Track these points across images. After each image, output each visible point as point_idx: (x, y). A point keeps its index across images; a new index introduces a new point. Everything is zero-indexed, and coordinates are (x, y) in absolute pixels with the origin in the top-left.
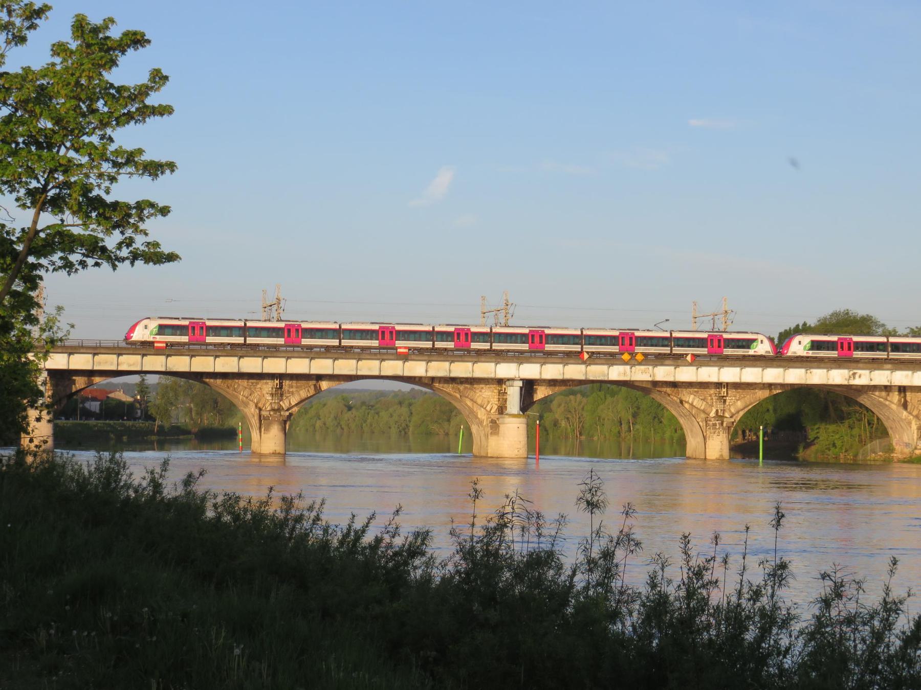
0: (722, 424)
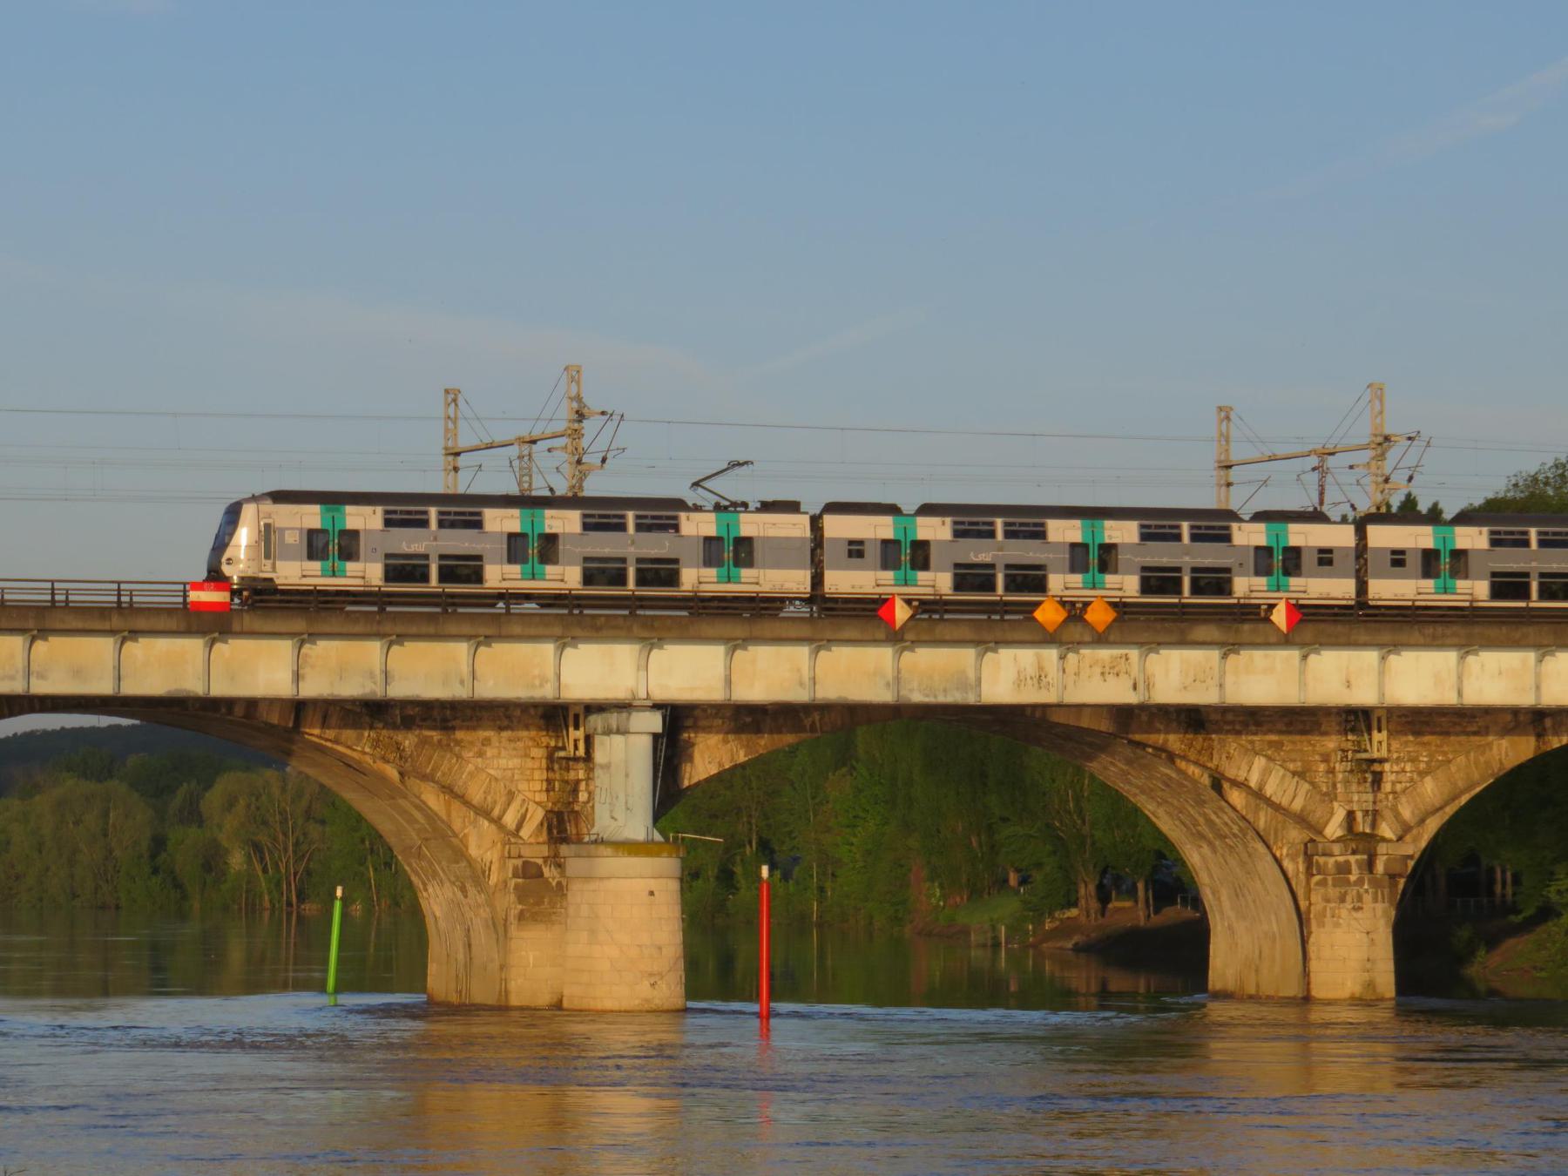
0: (1370, 865)
